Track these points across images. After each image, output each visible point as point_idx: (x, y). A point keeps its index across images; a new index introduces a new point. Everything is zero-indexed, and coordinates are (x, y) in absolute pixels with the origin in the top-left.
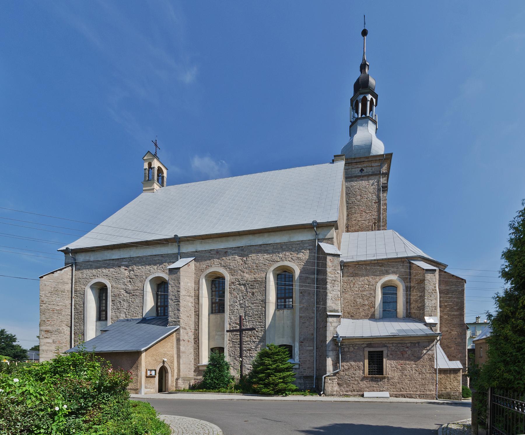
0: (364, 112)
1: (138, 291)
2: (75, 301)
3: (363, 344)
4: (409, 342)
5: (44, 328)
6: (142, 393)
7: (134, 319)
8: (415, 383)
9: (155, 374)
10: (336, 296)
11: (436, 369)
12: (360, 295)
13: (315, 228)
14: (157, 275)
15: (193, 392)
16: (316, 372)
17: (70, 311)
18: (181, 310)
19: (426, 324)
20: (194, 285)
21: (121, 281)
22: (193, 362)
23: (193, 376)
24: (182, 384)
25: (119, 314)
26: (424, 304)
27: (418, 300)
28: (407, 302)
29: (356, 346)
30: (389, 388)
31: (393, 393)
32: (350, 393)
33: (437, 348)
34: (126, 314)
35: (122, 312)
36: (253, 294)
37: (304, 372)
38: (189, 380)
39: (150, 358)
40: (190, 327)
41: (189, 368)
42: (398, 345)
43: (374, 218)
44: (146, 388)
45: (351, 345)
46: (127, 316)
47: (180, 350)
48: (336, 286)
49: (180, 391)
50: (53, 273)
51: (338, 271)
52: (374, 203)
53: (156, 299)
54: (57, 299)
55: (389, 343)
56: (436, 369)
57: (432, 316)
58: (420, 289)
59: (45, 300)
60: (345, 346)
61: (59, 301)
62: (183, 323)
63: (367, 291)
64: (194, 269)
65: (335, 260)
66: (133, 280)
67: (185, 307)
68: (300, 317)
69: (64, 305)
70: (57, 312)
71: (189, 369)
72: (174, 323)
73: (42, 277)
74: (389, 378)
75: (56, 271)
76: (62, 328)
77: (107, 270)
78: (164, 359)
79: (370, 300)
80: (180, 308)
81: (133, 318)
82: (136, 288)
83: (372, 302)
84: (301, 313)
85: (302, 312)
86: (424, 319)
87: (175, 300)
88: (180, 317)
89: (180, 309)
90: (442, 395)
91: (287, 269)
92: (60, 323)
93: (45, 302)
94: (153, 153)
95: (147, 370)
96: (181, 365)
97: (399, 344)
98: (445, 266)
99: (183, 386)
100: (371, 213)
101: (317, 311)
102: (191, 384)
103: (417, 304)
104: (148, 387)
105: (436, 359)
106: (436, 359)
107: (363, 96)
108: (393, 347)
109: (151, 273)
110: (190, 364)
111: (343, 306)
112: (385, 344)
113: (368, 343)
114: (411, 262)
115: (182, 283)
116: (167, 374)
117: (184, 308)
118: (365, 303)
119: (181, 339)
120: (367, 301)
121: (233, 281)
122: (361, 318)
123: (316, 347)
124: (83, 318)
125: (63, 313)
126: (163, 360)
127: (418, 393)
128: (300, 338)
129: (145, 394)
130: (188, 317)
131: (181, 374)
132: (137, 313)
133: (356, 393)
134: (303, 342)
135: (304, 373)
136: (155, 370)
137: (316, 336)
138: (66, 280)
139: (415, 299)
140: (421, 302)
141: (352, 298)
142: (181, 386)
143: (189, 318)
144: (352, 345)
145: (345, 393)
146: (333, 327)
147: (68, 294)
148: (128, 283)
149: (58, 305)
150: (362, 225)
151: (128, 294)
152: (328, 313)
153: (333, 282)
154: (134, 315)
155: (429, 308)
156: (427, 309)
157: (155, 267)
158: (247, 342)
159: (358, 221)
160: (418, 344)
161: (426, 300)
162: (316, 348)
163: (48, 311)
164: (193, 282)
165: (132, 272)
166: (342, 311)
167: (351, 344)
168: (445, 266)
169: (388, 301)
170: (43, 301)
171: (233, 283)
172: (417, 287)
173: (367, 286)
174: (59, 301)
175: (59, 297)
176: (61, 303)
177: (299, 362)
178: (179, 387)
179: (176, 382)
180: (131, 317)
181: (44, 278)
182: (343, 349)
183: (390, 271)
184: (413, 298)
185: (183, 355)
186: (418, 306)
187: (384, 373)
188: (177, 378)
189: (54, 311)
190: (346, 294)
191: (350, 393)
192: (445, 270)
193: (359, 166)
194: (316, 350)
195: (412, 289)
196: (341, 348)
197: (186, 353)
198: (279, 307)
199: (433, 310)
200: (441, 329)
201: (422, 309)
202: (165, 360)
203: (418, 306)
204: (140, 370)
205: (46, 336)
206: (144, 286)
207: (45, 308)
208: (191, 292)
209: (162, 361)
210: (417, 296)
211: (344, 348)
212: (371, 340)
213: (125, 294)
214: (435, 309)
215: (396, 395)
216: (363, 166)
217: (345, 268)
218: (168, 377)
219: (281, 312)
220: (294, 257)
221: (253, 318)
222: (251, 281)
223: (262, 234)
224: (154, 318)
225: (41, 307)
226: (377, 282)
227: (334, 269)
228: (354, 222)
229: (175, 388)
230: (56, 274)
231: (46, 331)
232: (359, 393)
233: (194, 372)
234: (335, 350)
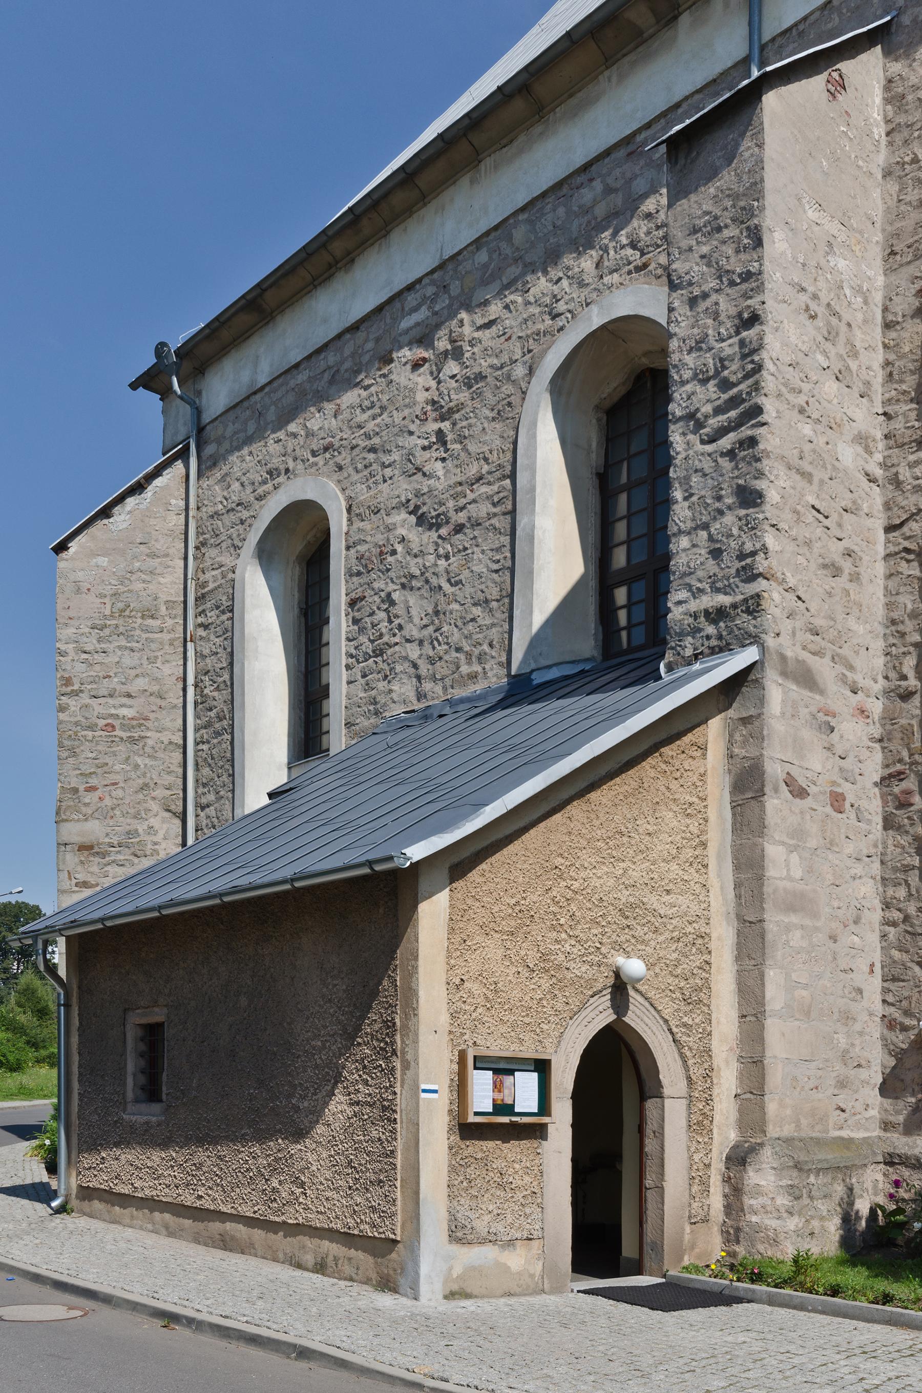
1: (484, 489)
2: (200, 656)
5: (74, 831)
6: (424, 1288)
7: (462, 701)
9: (544, 1106)
14: (596, 318)
15: (887, 1299)
17: (180, 721)
18: (772, 496)
20: (880, 280)
21: (396, 456)
22: (878, 998)
23: (877, 1132)
24: (783, 1201)
25: (382, 685)
34: (419, 678)
35: (399, 668)
38: (844, 1170)
39: (493, 949)
40: (851, 668)
41: (844, 1057)
44: (459, 1241)
46: (427, 686)
47: (760, 879)
49: (756, 1278)
50: (105, 513)
53: (594, 520)
54: (128, 660)
59: (77, 670)
61: (133, 673)
62: (786, 626)
64: (879, 131)
66: (454, 424)
67: (807, 476)
69: (155, 688)
70: (124, 735)
71: (838, 1066)
72: (711, 630)
73: (61, 547)
75: (121, 499)
77: (329, 407)
78: (620, 960)
80: (760, 475)
81: (459, 693)
82: (473, 470)
87: (718, 411)
88: (761, 565)
89: (761, 485)
92: (141, 796)
93: (76, 687)
95: (462, 1055)
96: (773, 1029)
99: (793, 1223)
102: (863, 1207)
104: (481, 1225)
109: (560, 322)
110: (847, 1018)
115: (778, 235)
116: (650, 1104)
117: (801, 483)
119: (774, 770)
124: (228, 755)
125: (153, 737)
126: (617, 974)
129: (451, 1296)
130: (836, 572)
131: (771, 1107)
132: (476, 652)
136: (542, 1067)
138: (160, 545)
143: (842, 582)
147: (170, 622)
148: (427, 454)
151: (431, 527)
154: (465, 669)
157: (587, 264)
163: (90, 734)
164: (876, 254)
165: (452, 367)
170: (68, 682)
174: (133, 673)
175: (134, 645)
178: (757, 1229)
179: (727, 1180)
180: (445, 689)
181: (74, 546)
185: (788, 928)
188: (735, 1147)
197: (815, 915)
200: (660, 1112)
202: (634, 967)
204: (406, 1066)
205: (81, 877)
206: (515, 443)
207: (79, 718)
208: (859, 338)
209: (605, 980)
213: (418, 538)
218: (660, 1134)
224: (582, 672)
225: (62, 716)
229: (717, 1240)
230: (121, 518)
231: (83, 848)
233: (886, 1089)
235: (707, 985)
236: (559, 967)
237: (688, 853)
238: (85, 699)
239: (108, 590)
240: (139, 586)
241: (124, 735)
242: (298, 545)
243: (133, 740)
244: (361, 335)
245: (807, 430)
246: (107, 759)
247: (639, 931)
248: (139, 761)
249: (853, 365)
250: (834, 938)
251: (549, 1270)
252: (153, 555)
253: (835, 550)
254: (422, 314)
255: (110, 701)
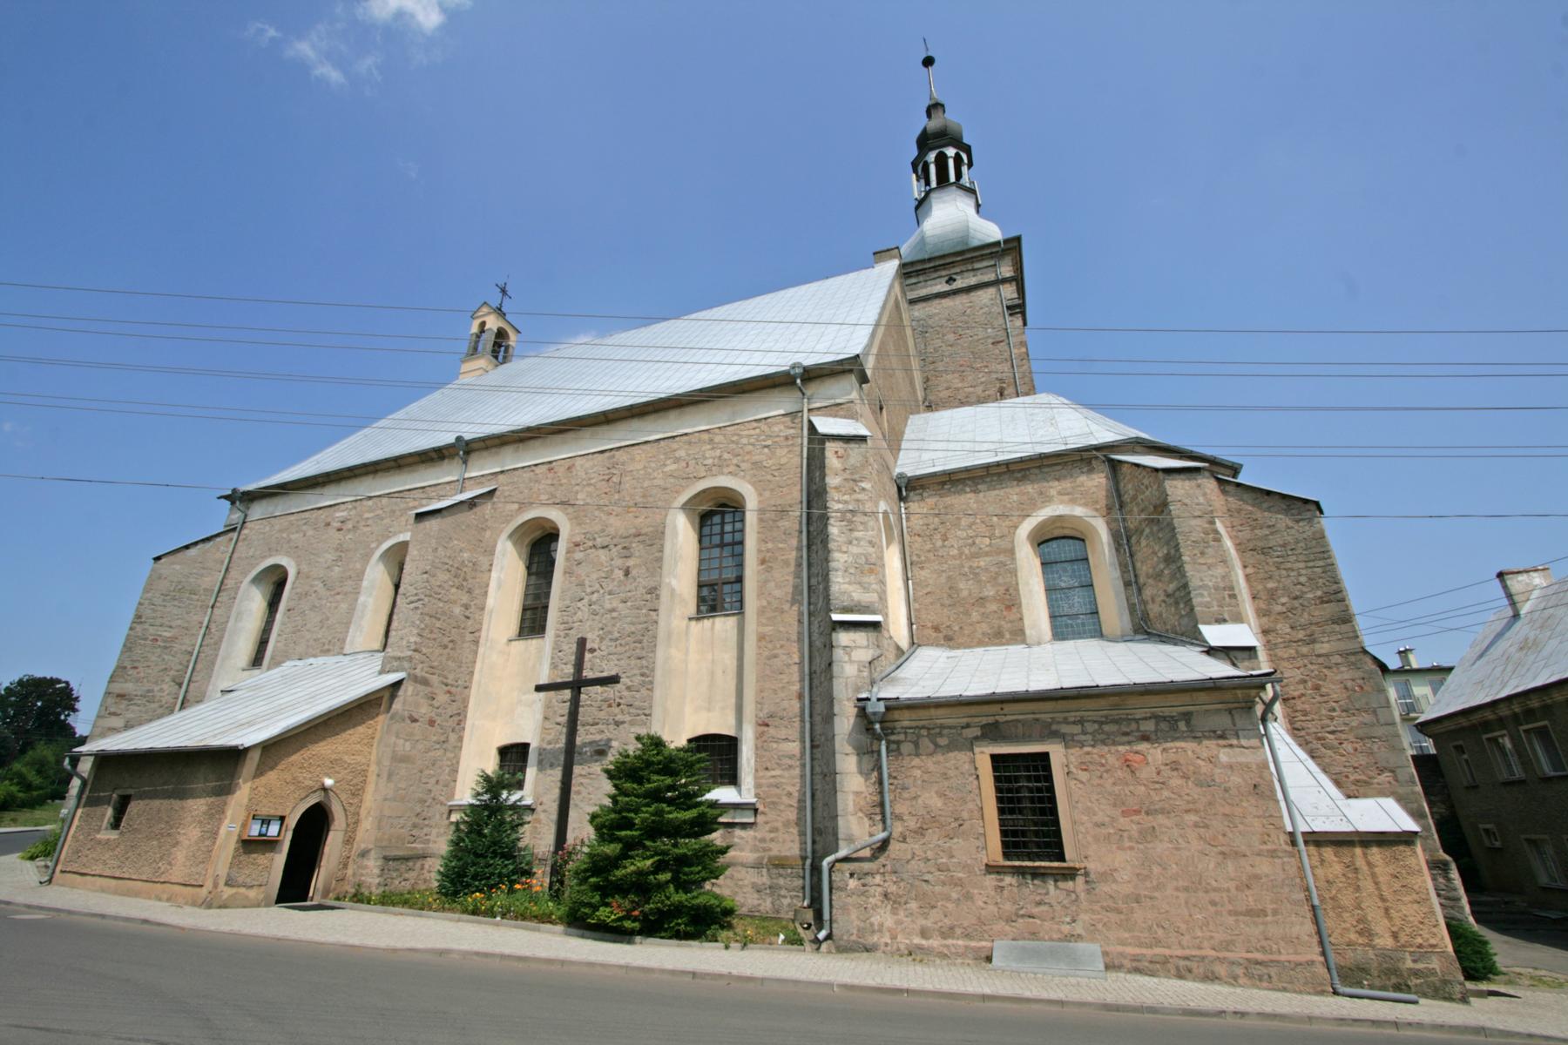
0: (943, 179)
3: (968, 726)
4: (1147, 712)
8: (1214, 903)
10: (862, 561)
11: (1292, 834)
12: (966, 569)
13: (799, 381)
16: (814, 842)
19: (1212, 651)
26: (1183, 581)
27: (1162, 571)
28: (1127, 584)
29: (940, 735)
30: (1100, 926)
31: (1120, 949)
32: (935, 943)
33: (1277, 744)
36: (627, 573)
37: (772, 840)
40: (446, 678)
42: (1106, 728)
43: (997, 379)
45: (924, 732)
48: (861, 528)
51: (863, 485)
52: (993, 343)
55: (1066, 721)
56: (1292, 834)
57: (1224, 621)
58: (1161, 535)
60: (902, 737)
63: (987, 554)
65: (850, 452)
68: (761, 638)
69: (186, 625)
74: (1092, 876)
76: (159, 688)
79: (1000, 585)
83: (1007, 590)
84: (763, 625)
85: (764, 621)
86: (1200, 633)
90: (1363, 970)
91: (728, 499)
94: (495, 304)
97: (1106, 723)
98: (1235, 470)
100: (987, 367)
101: (810, 614)
103: (1160, 584)
104: (240, 880)
105: (1280, 781)
106: (1280, 781)
107: (937, 151)
108: (1083, 738)
111: (917, 606)
112: (1051, 724)
113: (985, 720)
114: (1113, 460)
118: (986, 594)
120: (993, 586)
121: (578, 539)
122: (980, 644)
123: (812, 741)
127: (1238, 954)
128: (759, 703)
133: (960, 942)
134: (767, 725)
135: (772, 845)
137: (811, 702)
139: (1151, 571)
140: (1173, 577)
141: (943, 579)
142: (370, 880)
144: (929, 729)
145: (917, 940)
146: (856, 667)
149: (171, 627)
150: (967, 397)
152: (836, 617)
153: (849, 515)
155: (1206, 593)
156: (1202, 595)
158: (597, 724)
159: (958, 389)
160: (1188, 723)
161: (1187, 567)
162: (813, 747)
163: (143, 642)
166: (913, 620)
167: (923, 727)
168: (1235, 470)
169: (1063, 585)
171: (577, 545)
172: (1147, 531)
173: (987, 541)
176: (179, 622)
177: (754, 800)
182: (893, 746)
183: (1053, 492)
184: (1144, 569)
186: (1165, 591)
187: (1069, 852)
189: (157, 640)
190: (922, 568)
191: (935, 943)
192: (1239, 480)
193: (944, 273)
194: (812, 753)
195: (1133, 540)
196: (888, 743)
198: (703, 608)
199: (1224, 598)
201: (1182, 597)
202: (329, 782)
203: (1165, 591)
205: (112, 710)
210: (1155, 559)
211: (898, 743)
212: (995, 708)
214: (1233, 596)
215: (1135, 959)
216: (953, 271)
217: (912, 494)
219: (707, 623)
220: (743, 461)
221: (621, 645)
222: (625, 538)
223: (661, 414)
226: (1016, 527)
227: (849, 477)
228: (945, 392)
232: (973, 944)
234: (868, 753)
235: (363, 789)
236: (299, 782)
237: (366, 741)
238: (146, 626)
239: (176, 580)
240: (192, 580)
241: (162, 644)
242: (275, 578)
243: (166, 648)
244: (321, 512)
245: (441, 605)
246: (149, 655)
247: (337, 769)
248: (166, 657)
249: (465, 583)
250: (421, 772)
251: (266, 898)
252: (204, 568)
253: (446, 640)
254: (344, 514)
255: (160, 628)
